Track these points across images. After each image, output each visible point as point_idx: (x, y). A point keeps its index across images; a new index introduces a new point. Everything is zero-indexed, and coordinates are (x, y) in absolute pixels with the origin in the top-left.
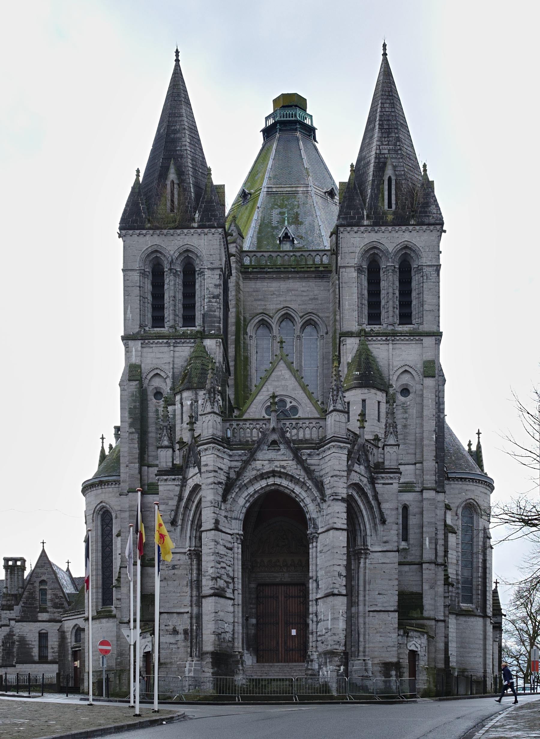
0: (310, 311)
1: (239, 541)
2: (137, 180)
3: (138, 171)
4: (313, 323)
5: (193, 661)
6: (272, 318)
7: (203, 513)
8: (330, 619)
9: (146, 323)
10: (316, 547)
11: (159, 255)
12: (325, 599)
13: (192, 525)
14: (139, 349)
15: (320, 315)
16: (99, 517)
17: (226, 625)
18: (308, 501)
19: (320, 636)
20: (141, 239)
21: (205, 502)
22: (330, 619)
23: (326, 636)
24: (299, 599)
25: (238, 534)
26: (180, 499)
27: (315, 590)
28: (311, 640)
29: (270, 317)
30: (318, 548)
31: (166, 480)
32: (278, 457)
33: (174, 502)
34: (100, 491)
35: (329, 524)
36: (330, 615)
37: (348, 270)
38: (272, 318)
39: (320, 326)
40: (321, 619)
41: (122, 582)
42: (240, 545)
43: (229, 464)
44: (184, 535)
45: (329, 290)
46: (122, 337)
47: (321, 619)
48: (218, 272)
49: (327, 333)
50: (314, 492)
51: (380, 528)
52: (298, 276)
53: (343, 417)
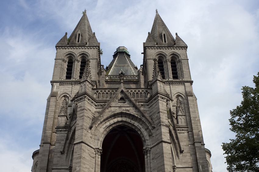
1: (99, 154)
3: (66, 34)
10: (150, 157)
11: (71, 55)
18: (143, 130)
20: (64, 50)
21: (78, 127)
25: (99, 149)
26: (67, 139)
30: (151, 157)
31: (61, 131)
33: (63, 142)
42: (100, 156)
43: (95, 110)
44: (68, 157)
46: (51, 81)
50: (147, 124)
51: (181, 155)
53: (162, 84)
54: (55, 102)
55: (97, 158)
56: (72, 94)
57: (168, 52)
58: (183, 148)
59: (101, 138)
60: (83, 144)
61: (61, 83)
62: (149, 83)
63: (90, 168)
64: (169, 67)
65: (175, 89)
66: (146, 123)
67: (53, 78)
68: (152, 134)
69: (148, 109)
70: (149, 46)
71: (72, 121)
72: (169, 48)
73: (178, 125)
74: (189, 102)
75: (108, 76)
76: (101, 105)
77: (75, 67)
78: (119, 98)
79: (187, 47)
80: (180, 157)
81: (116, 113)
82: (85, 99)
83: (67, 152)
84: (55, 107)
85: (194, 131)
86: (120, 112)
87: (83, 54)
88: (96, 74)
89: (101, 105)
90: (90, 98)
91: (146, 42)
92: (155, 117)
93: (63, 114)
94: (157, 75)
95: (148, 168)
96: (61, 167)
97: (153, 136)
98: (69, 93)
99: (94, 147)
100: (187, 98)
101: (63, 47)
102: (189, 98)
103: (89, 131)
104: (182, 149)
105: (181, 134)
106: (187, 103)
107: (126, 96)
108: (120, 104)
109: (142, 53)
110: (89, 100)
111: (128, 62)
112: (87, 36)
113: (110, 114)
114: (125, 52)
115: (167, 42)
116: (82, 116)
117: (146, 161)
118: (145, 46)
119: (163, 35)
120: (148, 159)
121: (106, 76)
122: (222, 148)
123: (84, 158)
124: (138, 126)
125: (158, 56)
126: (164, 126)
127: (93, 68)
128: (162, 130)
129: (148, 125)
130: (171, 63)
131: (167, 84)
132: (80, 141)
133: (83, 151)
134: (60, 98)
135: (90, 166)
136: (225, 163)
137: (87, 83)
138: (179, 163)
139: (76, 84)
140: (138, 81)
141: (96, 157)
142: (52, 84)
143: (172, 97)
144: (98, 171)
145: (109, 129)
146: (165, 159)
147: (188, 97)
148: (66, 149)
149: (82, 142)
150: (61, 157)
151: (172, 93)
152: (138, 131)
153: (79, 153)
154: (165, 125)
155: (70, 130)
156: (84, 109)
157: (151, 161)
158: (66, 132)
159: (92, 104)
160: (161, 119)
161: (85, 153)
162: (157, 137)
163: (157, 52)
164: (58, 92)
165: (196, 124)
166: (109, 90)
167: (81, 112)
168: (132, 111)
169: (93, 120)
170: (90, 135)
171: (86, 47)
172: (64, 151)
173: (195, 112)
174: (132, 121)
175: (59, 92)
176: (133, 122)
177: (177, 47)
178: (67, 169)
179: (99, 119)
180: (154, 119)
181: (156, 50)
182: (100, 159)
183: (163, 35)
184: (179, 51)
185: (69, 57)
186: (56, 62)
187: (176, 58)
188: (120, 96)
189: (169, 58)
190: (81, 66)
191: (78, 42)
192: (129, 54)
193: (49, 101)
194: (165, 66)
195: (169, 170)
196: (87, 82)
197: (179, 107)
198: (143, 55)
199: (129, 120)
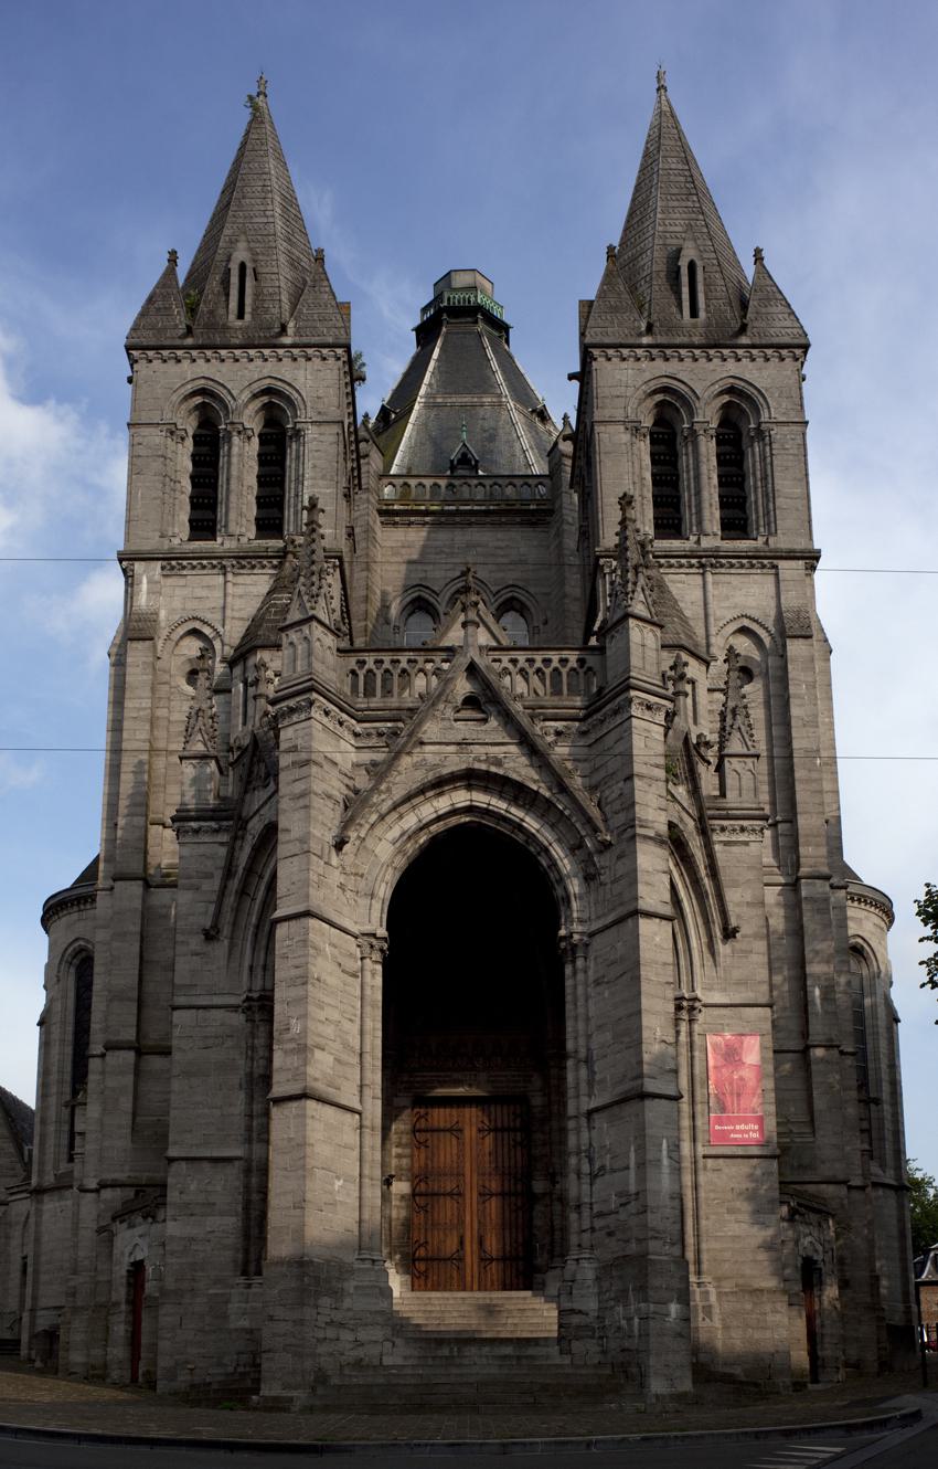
0: (511, 583)
1: (377, 956)
2: (171, 271)
3: (173, 258)
4: (518, 606)
5: (249, 1286)
6: (438, 595)
7: (280, 874)
8: (632, 1165)
9: (176, 530)
10: (586, 972)
12: (616, 1109)
13: (256, 935)
14: (157, 577)
15: (532, 590)
16: (72, 970)
17: (339, 1183)
18: (557, 851)
19: (601, 1215)
21: (288, 842)
22: (632, 1165)
23: (622, 1216)
24: (512, 1135)
25: (374, 935)
26: (229, 872)
27: (584, 1087)
28: (574, 1226)
29: (434, 591)
30: (591, 973)
31: (196, 832)
32: (481, 736)
33: (214, 884)
34: (75, 916)
35: (622, 904)
36: (632, 1155)
37: (611, 428)
38: (438, 595)
39: (533, 610)
40: (602, 1168)
41: (89, 1092)
42: (379, 968)
43: (354, 757)
45: (548, 547)
46: (119, 553)
47: (602, 1168)
48: (336, 429)
49: (546, 623)
50: (578, 825)
51: (723, 949)
52: (488, 520)
54: (149, 670)
55: (368, 975)
56: (227, 622)
57: (704, 378)
58: (738, 917)
59: (383, 885)
60: (313, 922)
61: (173, 562)
62: (602, 561)
63: (342, 1020)
64: (704, 469)
65: (727, 598)
66: (574, 819)
67: (127, 534)
68: (600, 874)
69: (586, 750)
70: (607, 340)
71: (246, 792)
72: (712, 352)
73: (721, 803)
74: (790, 667)
75: (394, 481)
76: (380, 735)
77: (234, 472)
78: (460, 699)
79: (806, 347)
80: (721, 959)
81: (445, 771)
82: (313, 714)
83: (233, 931)
84: (150, 695)
85: (802, 821)
86: (464, 766)
87: (268, 391)
88: (340, 496)
89: (380, 735)
90: (332, 707)
91: (599, 296)
92: (614, 795)
93: (200, 747)
94: (630, 585)
95: (576, 1018)
96: (208, 997)
97: (601, 884)
98: (215, 618)
99: (355, 929)
100: (784, 646)
101: (164, 348)
102: (795, 648)
103: (335, 861)
104: (733, 922)
105: (735, 849)
106: (779, 673)
107: (488, 692)
108: (464, 730)
109: (571, 377)
110: (327, 713)
111: (500, 377)
112: (281, 278)
113: (421, 777)
114: (479, 309)
115: (702, 314)
116: (304, 794)
117: (568, 990)
118: (588, 340)
119: (684, 271)
120: (579, 980)
121: (381, 477)
122: (918, 914)
123: (318, 980)
124: (538, 835)
125: (650, 403)
126: (650, 842)
127: (323, 478)
128: (638, 862)
129: (583, 833)
130: (718, 444)
131: (692, 566)
132: (301, 908)
133: (312, 951)
134: (170, 644)
135: (343, 1013)
136: (923, 986)
137: (318, 631)
138: (715, 986)
139: (243, 567)
140: (551, 512)
141: (362, 970)
142: (124, 571)
143: (713, 640)
144: (374, 1029)
145: (416, 842)
146: (644, 987)
147: (788, 641)
148: (227, 917)
149: (308, 914)
150: (204, 954)
151: (711, 619)
152: (539, 854)
153: (296, 962)
154: (650, 838)
155: (240, 833)
156: (307, 763)
157: (589, 989)
158: (224, 838)
159: (339, 730)
160: (637, 808)
161: (320, 959)
162: (617, 888)
163: (648, 376)
164: (157, 614)
165: (814, 786)
166: (411, 655)
167: (297, 773)
168: (517, 766)
169: (346, 807)
170: (336, 877)
171: (281, 351)
172: (216, 926)
173: (813, 722)
174: (513, 810)
175: (163, 614)
176: (517, 813)
177: (754, 346)
178: (234, 1008)
179: (375, 800)
180: (607, 804)
181: (644, 364)
182: (379, 981)
183: (684, 271)
184: (765, 373)
185: (197, 407)
186: (137, 440)
187: (743, 411)
188: (463, 687)
189: (708, 415)
190: (263, 459)
191: (241, 315)
192: (506, 319)
193: (119, 662)
194: (685, 461)
195: (658, 1034)
196: (314, 624)
197: (734, 712)
198: (576, 384)
199: (499, 805)
